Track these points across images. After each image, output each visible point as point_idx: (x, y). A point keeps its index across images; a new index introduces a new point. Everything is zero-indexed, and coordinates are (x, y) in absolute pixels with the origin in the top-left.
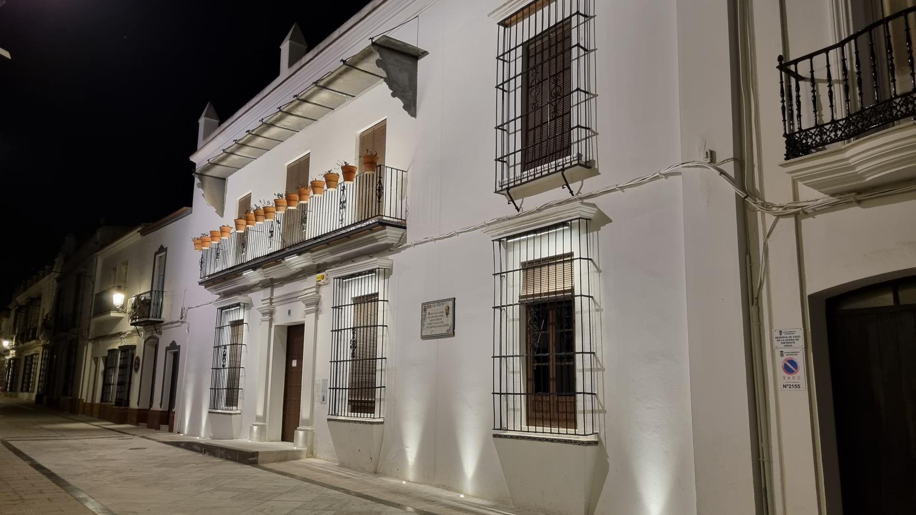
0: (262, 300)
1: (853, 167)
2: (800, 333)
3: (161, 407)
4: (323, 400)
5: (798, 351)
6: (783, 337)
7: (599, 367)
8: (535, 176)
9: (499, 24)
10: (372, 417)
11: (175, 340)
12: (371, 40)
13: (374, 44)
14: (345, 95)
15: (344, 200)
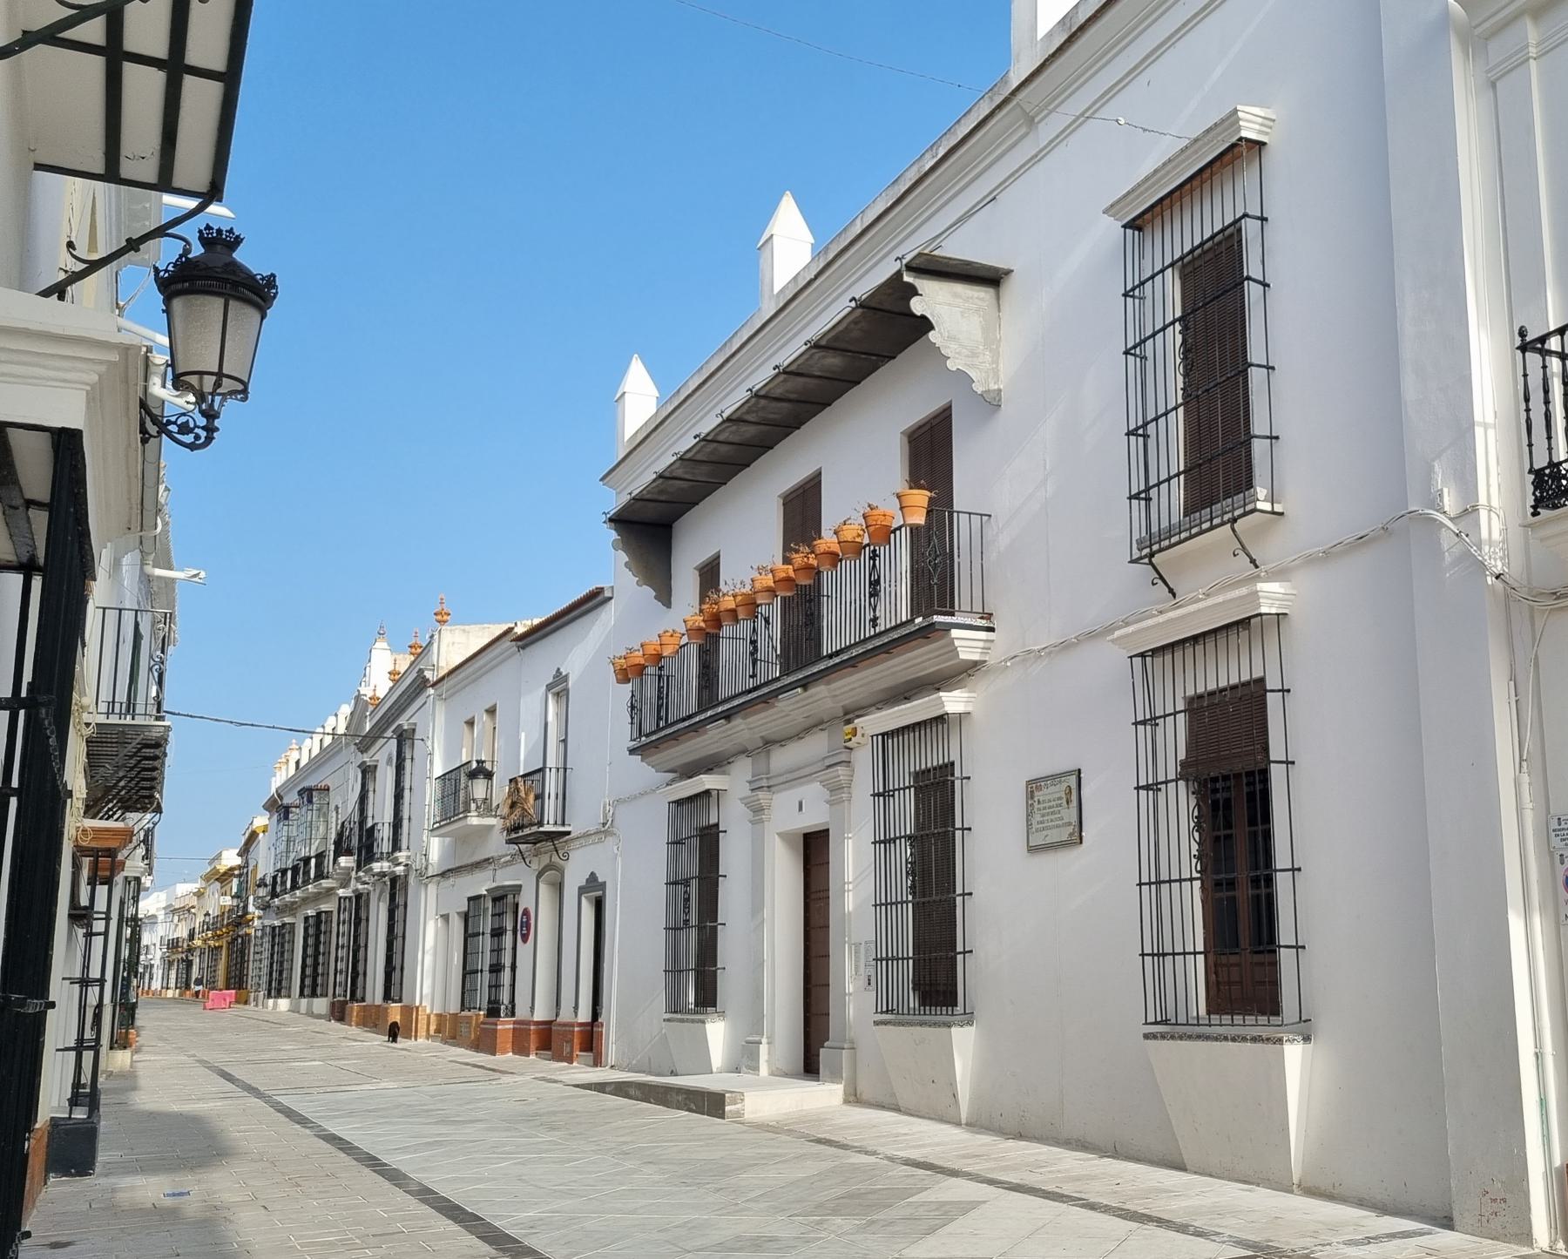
4: (869, 984)
6: (1563, 829)
8: (1211, 523)
9: (1125, 226)
10: (950, 1013)
11: (596, 872)
12: (898, 261)
14: (874, 358)
15: (876, 577)
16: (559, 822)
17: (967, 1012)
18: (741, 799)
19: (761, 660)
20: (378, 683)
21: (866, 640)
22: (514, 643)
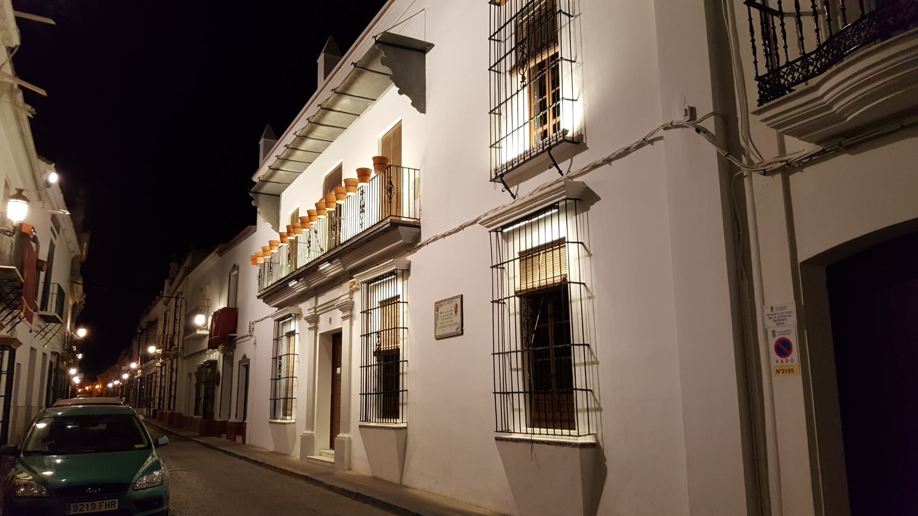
0: (309, 310)
1: (830, 107)
2: (792, 308)
3: (236, 419)
5: (790, 330)
6: (775, 314)
7: (594, 360)
12: (374, 38)
13: (377, 42)
14: (365, 100)
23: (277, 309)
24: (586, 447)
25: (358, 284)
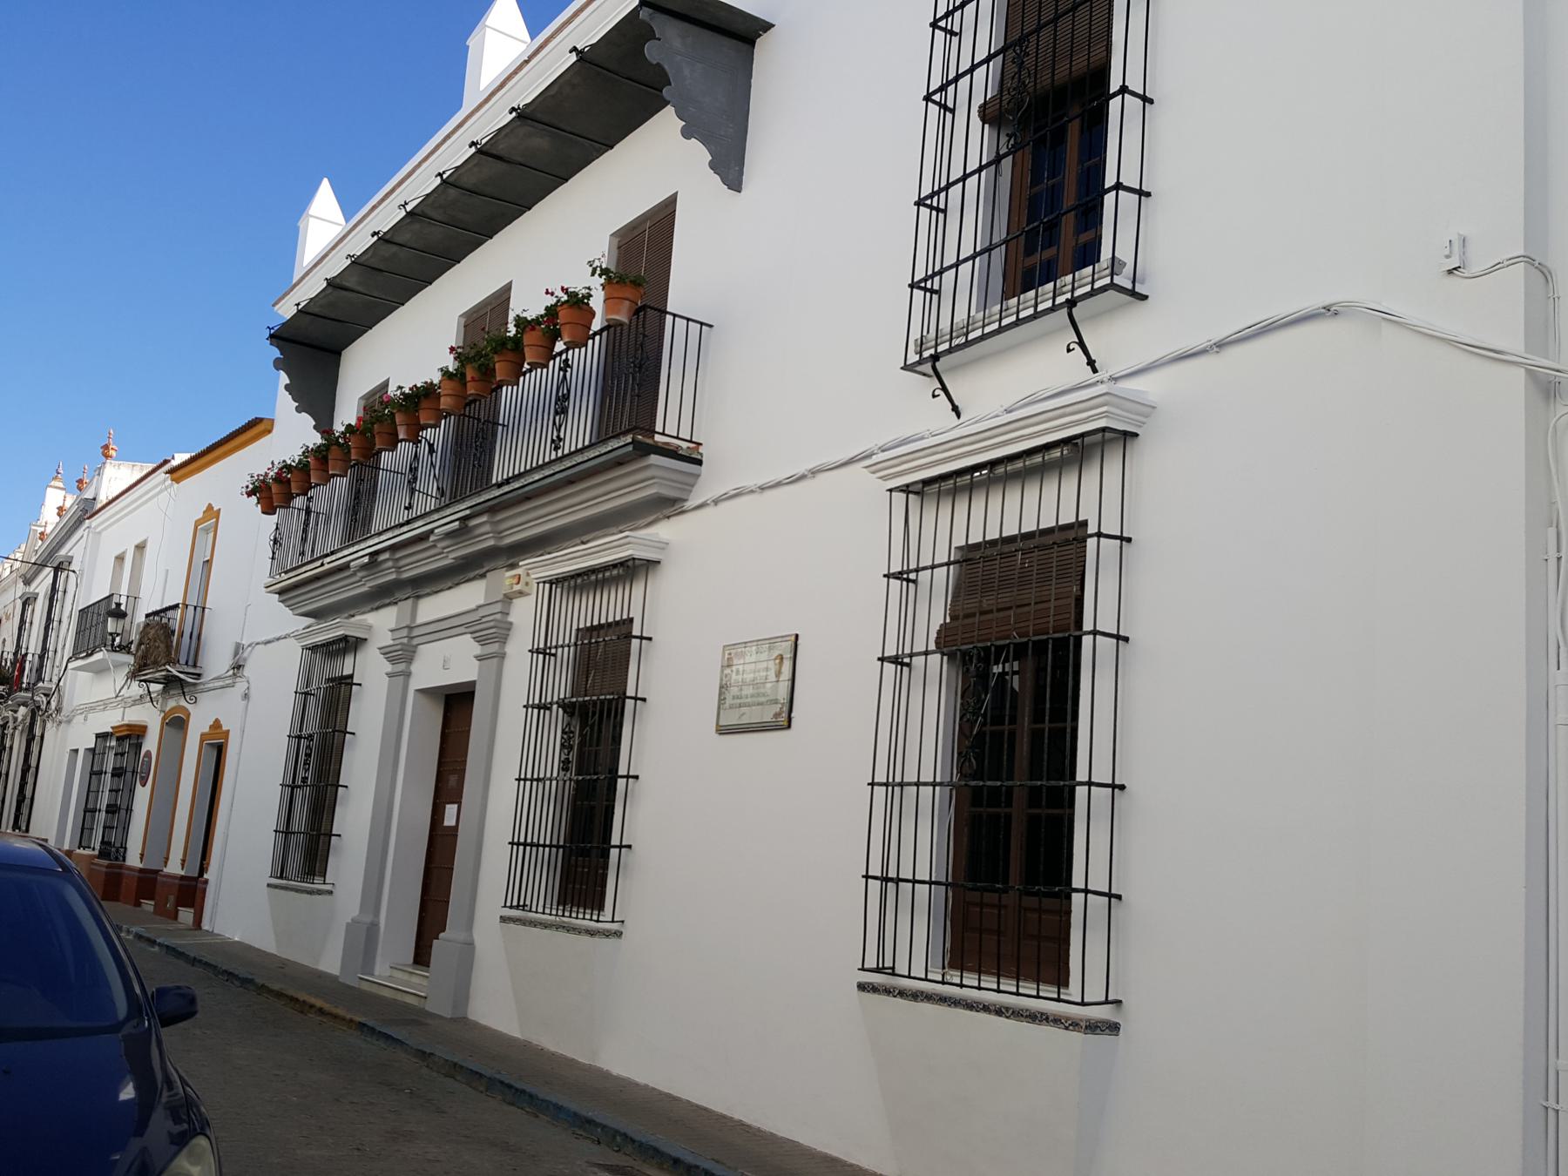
3: (182, 869)
10: (595, 917)
11: (149, 727)
15: (565, 391)
16: (190, 663)
17: (615, 919)
18: (380, 649)
19: (419, 492)
20: (49, 519)
21: (545, 465)
22: (167, 475)
23: (310, 621)
24: (1098, 1031)
25: (527, 584)
